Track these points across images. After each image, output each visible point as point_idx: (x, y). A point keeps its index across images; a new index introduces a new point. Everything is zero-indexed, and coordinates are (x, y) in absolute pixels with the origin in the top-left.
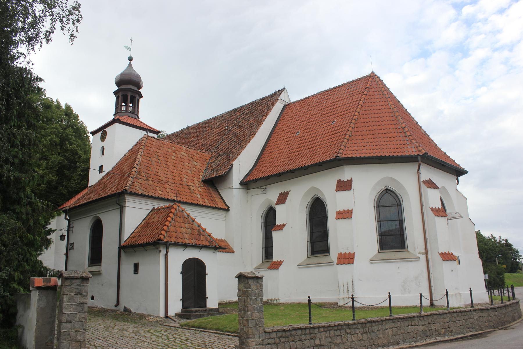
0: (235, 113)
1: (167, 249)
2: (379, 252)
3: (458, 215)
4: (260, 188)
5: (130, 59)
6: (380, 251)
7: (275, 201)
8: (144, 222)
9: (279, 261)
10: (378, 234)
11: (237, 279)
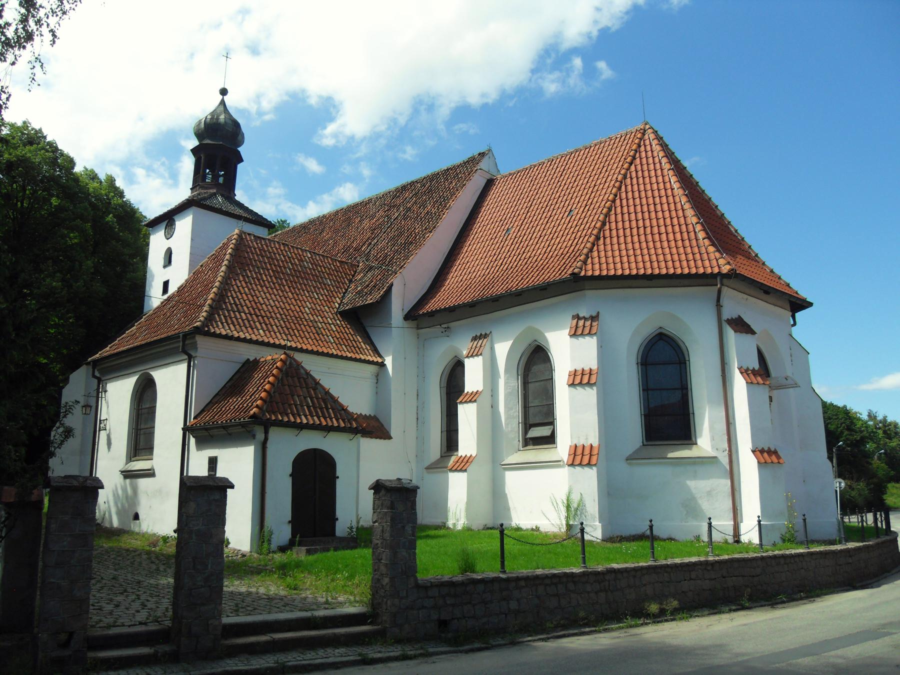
0: (402, 192)
1: (266, 433)
2: (643, 445)
3: (789, 382)
4: (439, 326)
5: (224, 92)
6: (645, 443)
7: (465, 353)
8: (230, 384)
9: (469, 455)
10: (643, 413)
11: (373, 491)
